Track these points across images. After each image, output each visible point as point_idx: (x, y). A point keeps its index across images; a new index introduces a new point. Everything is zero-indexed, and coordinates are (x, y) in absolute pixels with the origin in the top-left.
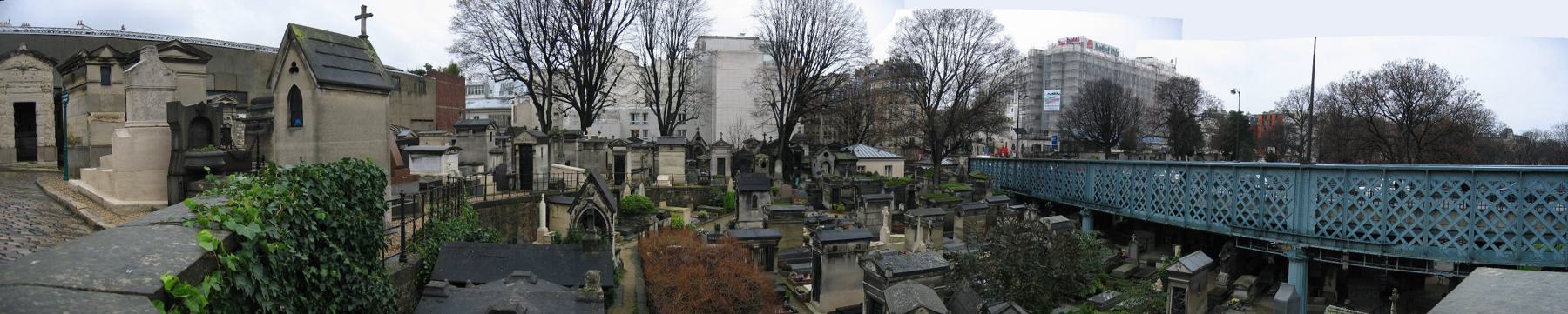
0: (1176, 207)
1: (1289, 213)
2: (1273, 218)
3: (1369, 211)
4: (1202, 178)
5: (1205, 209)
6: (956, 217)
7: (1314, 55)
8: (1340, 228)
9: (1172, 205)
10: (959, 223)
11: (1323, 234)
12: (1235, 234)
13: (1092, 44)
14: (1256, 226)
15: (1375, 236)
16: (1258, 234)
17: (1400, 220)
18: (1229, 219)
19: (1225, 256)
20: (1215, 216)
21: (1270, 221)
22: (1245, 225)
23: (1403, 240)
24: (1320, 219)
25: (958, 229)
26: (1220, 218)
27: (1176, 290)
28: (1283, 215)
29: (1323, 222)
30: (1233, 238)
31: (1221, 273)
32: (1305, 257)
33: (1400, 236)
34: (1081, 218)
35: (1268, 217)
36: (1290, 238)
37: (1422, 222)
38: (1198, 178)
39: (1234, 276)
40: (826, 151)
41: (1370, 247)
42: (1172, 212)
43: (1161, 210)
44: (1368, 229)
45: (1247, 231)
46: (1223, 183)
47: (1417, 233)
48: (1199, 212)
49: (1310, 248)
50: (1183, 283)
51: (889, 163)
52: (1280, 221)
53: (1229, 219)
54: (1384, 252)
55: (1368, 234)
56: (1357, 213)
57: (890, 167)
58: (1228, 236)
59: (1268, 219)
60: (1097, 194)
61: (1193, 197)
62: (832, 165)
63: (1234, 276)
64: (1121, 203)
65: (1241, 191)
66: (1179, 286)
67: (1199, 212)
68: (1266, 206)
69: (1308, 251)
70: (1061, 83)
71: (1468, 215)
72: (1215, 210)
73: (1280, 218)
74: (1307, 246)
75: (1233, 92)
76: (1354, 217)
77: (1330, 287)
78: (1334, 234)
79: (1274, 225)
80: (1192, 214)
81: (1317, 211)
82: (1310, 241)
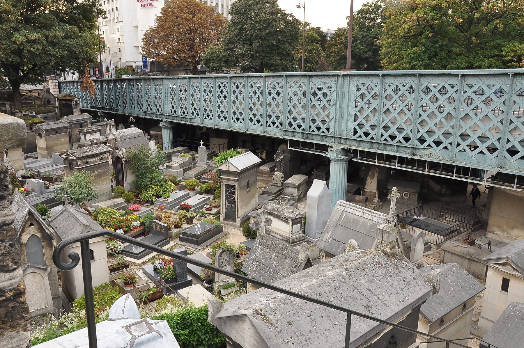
0: (238, 114)
1: (331, 117)
2: (319, 123)
3: (402, 115)
4: (300, 87)
5: (303, 119)
6: (38, 137)
8: (375, 131)
9: (235, 113)
10: (41, 143)
12: (286, 137)
14: (304, 130)
15: (407, 139)
16: (305, 136)
17: (431, 125)
18: (281, 124)
19: (279, 157)
21: (316, 124)
23: (433, 145)
24: (358, 122)
25: (41, 148)
26: (274, 123)
27: (228, 187)
28: (326, 119)
30: (285, 141)
31: (276, 173)
32: (343, 157)
33: (430, 141)
34: (160, 129)
35: (314, 121)
36: (332, 140)
37: (383, 120)
38: (296, 88)
41: (401, 150)
42: (235, 119)
43: (258, 122)
44: (400, 133)
45: (296, 134)
46: (276, 91)
47: (447, 138)
48: (297, 122)
50: (233, 180)
52: (324, 124)
54: (414, 154)
55: (400, 137)
56: (391, 117)
58: (242, 133)
59: (314, 123)
60: (173, 107)
61: (291, 107)
63: (287, 176)
64: (193, 113)
66: (230, 183)
67: (297, 122)
68: (312, 111)
69: (346, 152)
71: (501, 122)
72: (270, 116)
74: (346, 147)
76: (387, 121)
78: (370, 136)
79: (319, 128)
80: (251, 120)
81: (356, 115)
82: (349, 142)
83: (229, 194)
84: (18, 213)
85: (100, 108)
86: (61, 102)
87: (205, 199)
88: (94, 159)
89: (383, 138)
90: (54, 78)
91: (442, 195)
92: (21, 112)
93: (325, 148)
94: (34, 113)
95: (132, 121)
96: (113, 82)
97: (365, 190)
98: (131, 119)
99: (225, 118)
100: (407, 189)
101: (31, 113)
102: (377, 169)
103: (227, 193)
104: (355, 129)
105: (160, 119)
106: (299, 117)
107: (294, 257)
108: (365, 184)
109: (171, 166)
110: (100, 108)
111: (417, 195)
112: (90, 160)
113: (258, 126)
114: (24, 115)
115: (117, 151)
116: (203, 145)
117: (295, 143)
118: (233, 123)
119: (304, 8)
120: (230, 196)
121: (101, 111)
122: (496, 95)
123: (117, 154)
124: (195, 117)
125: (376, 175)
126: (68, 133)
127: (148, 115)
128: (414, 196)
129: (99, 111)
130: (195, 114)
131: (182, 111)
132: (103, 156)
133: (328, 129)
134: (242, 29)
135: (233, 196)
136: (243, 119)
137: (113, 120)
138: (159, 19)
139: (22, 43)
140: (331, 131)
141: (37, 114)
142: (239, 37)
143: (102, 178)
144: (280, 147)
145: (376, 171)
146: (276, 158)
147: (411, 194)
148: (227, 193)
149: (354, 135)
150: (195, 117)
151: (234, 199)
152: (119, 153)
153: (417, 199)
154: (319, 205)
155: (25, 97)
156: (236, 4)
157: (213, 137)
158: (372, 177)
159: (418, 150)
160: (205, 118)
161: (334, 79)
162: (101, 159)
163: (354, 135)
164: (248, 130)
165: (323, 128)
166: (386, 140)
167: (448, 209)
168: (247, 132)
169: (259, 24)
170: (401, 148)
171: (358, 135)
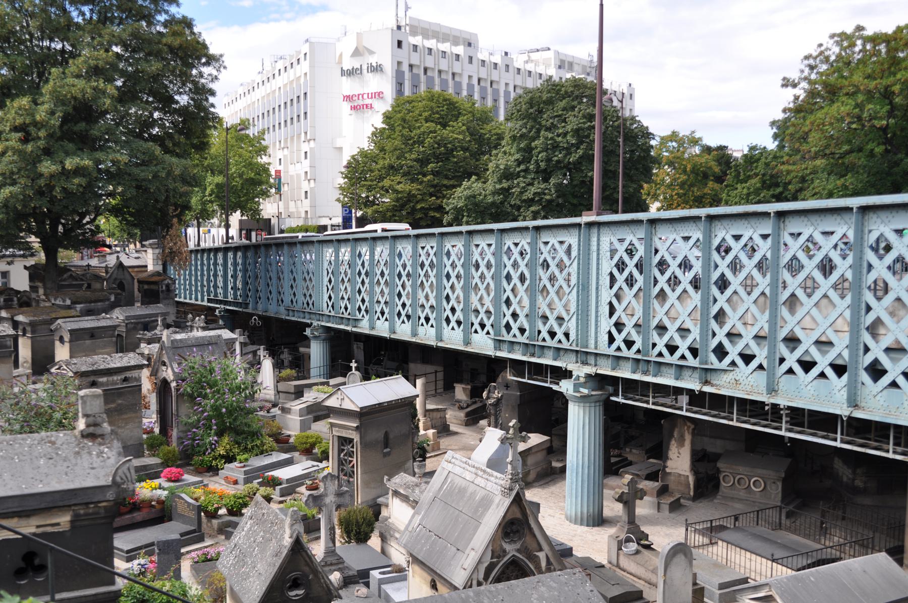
12: (500, 354)
20: (791, 361)
54: (707, 382)
69: (600, 380)
83: (344, 455)
85: (220, 302)
86: (141, 286)
87: (317, 468)
88: (110, 379)
90: (155, 244)
91: (856, 491)
92: (49, 300)
93: (562, 374)
94: (68, 302)
95: (255, 323)
96: (242, 249)
97: (668, 470)
98: (255, 319)
100: (759, 471)
101: (64, 301)
102: (689, 424)
103: (342, 455)
105: (309, 321)
106: (522, 311)
108: (667, 458)
109: (290, 409)
110: (220, 302)
111: (780, 484)
112: (101, 380)
114: (53, 304)
115: (164, 368)
116: (357, 369)
117: (518, 367)
118: (420, 327)
120: (346, 460)
121: (223, 306)
122: (894, 261)
123: (164, 375)
124: (363, 316)
125: (688, 438)
126: (114, 339)
127: (291, 313)
128: (774, 487)
129: (218, 308)
132: (128, 374)
133: (567, 335)
134: (529, 150)
135: (351, 461)
137: (203, 317)
138: (378, 134)
139: (52, 176)
141: (74, 303)
142: (522, 167)
143: (125, 416)
144: (500, 376)
145: (688, 429)
146: (488, 398)
147: (768, 483)
148: (342, 455)
150: (363, 316)
151: (353, 466)
152: (166, 371)
153: (780, 495)
155: (71, 275)
156: (518, 101)
157: (415, 361)
158: (681, 444)
159: (714, 374)
160: (378, 319)
161: (575, 232)
162: (126, 380)
164: (441, 340)
166: (660, 354)
167: (843, 518)
168: (440, 344)
169: (563, 138)
170: (686, 370)
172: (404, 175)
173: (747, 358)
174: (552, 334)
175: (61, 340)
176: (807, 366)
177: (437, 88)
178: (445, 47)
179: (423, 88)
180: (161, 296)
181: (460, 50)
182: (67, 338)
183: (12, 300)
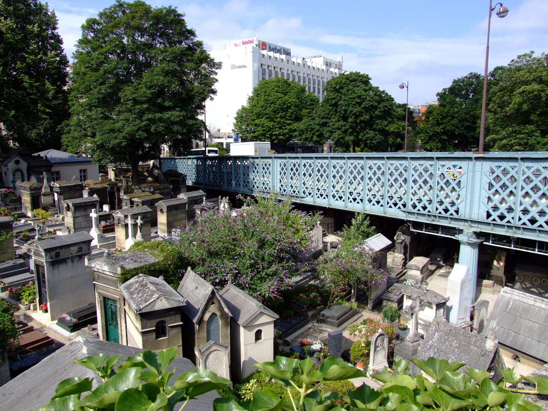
7: (488, 47)
11: (494, 220)
13: (266, 45)
20: (391, 203)
21: (353, 197)
22: (419, 210)
25: (161, 224)
29: (495, 208)
39: (408, 257)
40: (17, 158)
42: (351, 199)
43: (341, 198)
49: (480, 232)
51: (83, 167)
53: (404, 206)
57: (85, 171)
62: (25, 172)
63: (408, 257)
65: (442, 188)
69: (479, 235)
70: (203, 212)
73: (453, 204)
75: (402, 87)
77: (498, 265)
84: (197, 291)
89: (522, 222)
99: (341, 198)
104: (488, 212)
107: (480, 344)
113: (377, 207)
117: (417, 225)
119: (407, 87)
125: (503, 259)
130: (307, 193)
131: (292, 190)
136: (327, 196)
140: (460, 213)
149: (488, 218)
150: (307, 196)
154: (462, 290)
163: (488, 218)
165: (452, 210)
166: (440, 213)
168: (330, 207)
171: (491, 218)
172: (267, 118)
173: (310, 194)
174: (294, 192)
175: (162, 211)
176: (395, 204)
177: (286, 78)
178: (277, 55)
179: (273, 76)
180: (180, 183)
181: (283, 57)
182: (165, 210)
183: (114, 188)
